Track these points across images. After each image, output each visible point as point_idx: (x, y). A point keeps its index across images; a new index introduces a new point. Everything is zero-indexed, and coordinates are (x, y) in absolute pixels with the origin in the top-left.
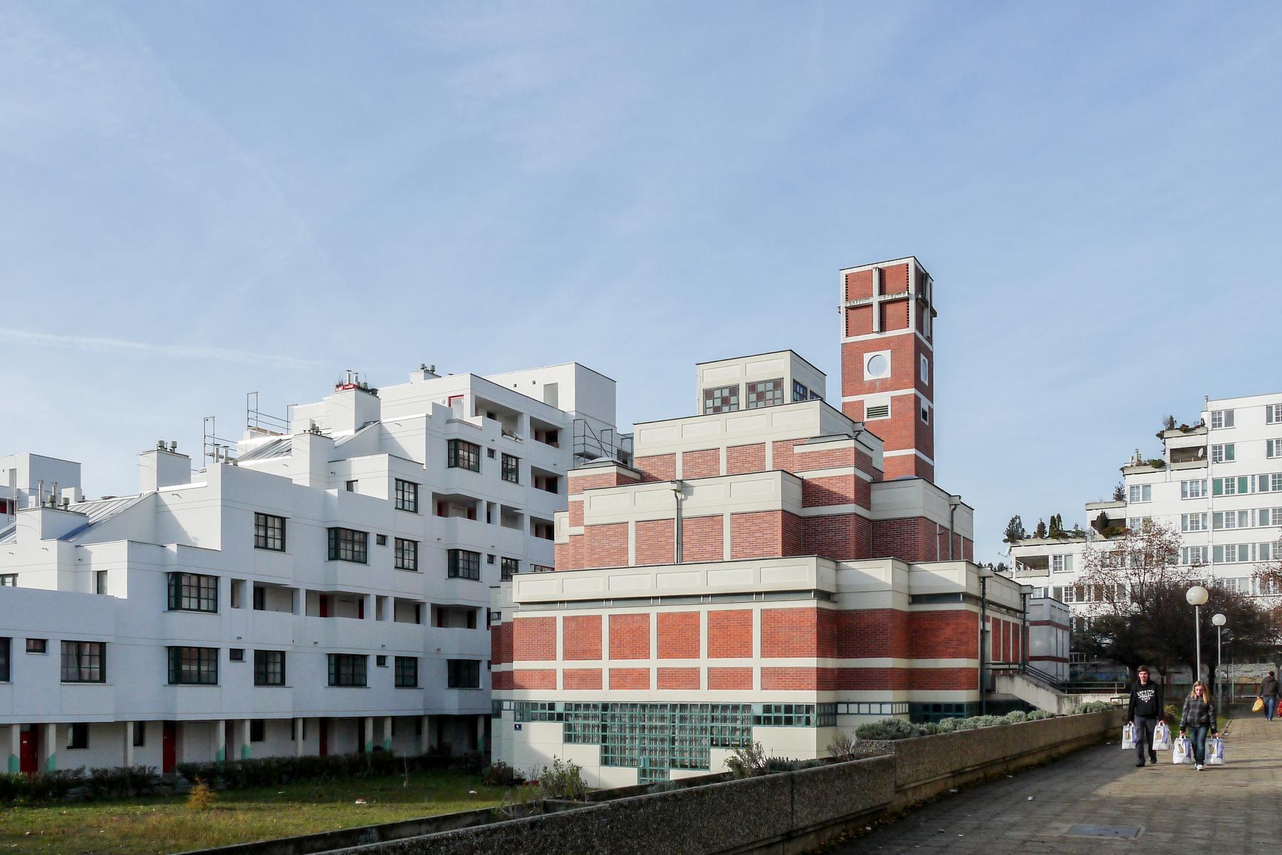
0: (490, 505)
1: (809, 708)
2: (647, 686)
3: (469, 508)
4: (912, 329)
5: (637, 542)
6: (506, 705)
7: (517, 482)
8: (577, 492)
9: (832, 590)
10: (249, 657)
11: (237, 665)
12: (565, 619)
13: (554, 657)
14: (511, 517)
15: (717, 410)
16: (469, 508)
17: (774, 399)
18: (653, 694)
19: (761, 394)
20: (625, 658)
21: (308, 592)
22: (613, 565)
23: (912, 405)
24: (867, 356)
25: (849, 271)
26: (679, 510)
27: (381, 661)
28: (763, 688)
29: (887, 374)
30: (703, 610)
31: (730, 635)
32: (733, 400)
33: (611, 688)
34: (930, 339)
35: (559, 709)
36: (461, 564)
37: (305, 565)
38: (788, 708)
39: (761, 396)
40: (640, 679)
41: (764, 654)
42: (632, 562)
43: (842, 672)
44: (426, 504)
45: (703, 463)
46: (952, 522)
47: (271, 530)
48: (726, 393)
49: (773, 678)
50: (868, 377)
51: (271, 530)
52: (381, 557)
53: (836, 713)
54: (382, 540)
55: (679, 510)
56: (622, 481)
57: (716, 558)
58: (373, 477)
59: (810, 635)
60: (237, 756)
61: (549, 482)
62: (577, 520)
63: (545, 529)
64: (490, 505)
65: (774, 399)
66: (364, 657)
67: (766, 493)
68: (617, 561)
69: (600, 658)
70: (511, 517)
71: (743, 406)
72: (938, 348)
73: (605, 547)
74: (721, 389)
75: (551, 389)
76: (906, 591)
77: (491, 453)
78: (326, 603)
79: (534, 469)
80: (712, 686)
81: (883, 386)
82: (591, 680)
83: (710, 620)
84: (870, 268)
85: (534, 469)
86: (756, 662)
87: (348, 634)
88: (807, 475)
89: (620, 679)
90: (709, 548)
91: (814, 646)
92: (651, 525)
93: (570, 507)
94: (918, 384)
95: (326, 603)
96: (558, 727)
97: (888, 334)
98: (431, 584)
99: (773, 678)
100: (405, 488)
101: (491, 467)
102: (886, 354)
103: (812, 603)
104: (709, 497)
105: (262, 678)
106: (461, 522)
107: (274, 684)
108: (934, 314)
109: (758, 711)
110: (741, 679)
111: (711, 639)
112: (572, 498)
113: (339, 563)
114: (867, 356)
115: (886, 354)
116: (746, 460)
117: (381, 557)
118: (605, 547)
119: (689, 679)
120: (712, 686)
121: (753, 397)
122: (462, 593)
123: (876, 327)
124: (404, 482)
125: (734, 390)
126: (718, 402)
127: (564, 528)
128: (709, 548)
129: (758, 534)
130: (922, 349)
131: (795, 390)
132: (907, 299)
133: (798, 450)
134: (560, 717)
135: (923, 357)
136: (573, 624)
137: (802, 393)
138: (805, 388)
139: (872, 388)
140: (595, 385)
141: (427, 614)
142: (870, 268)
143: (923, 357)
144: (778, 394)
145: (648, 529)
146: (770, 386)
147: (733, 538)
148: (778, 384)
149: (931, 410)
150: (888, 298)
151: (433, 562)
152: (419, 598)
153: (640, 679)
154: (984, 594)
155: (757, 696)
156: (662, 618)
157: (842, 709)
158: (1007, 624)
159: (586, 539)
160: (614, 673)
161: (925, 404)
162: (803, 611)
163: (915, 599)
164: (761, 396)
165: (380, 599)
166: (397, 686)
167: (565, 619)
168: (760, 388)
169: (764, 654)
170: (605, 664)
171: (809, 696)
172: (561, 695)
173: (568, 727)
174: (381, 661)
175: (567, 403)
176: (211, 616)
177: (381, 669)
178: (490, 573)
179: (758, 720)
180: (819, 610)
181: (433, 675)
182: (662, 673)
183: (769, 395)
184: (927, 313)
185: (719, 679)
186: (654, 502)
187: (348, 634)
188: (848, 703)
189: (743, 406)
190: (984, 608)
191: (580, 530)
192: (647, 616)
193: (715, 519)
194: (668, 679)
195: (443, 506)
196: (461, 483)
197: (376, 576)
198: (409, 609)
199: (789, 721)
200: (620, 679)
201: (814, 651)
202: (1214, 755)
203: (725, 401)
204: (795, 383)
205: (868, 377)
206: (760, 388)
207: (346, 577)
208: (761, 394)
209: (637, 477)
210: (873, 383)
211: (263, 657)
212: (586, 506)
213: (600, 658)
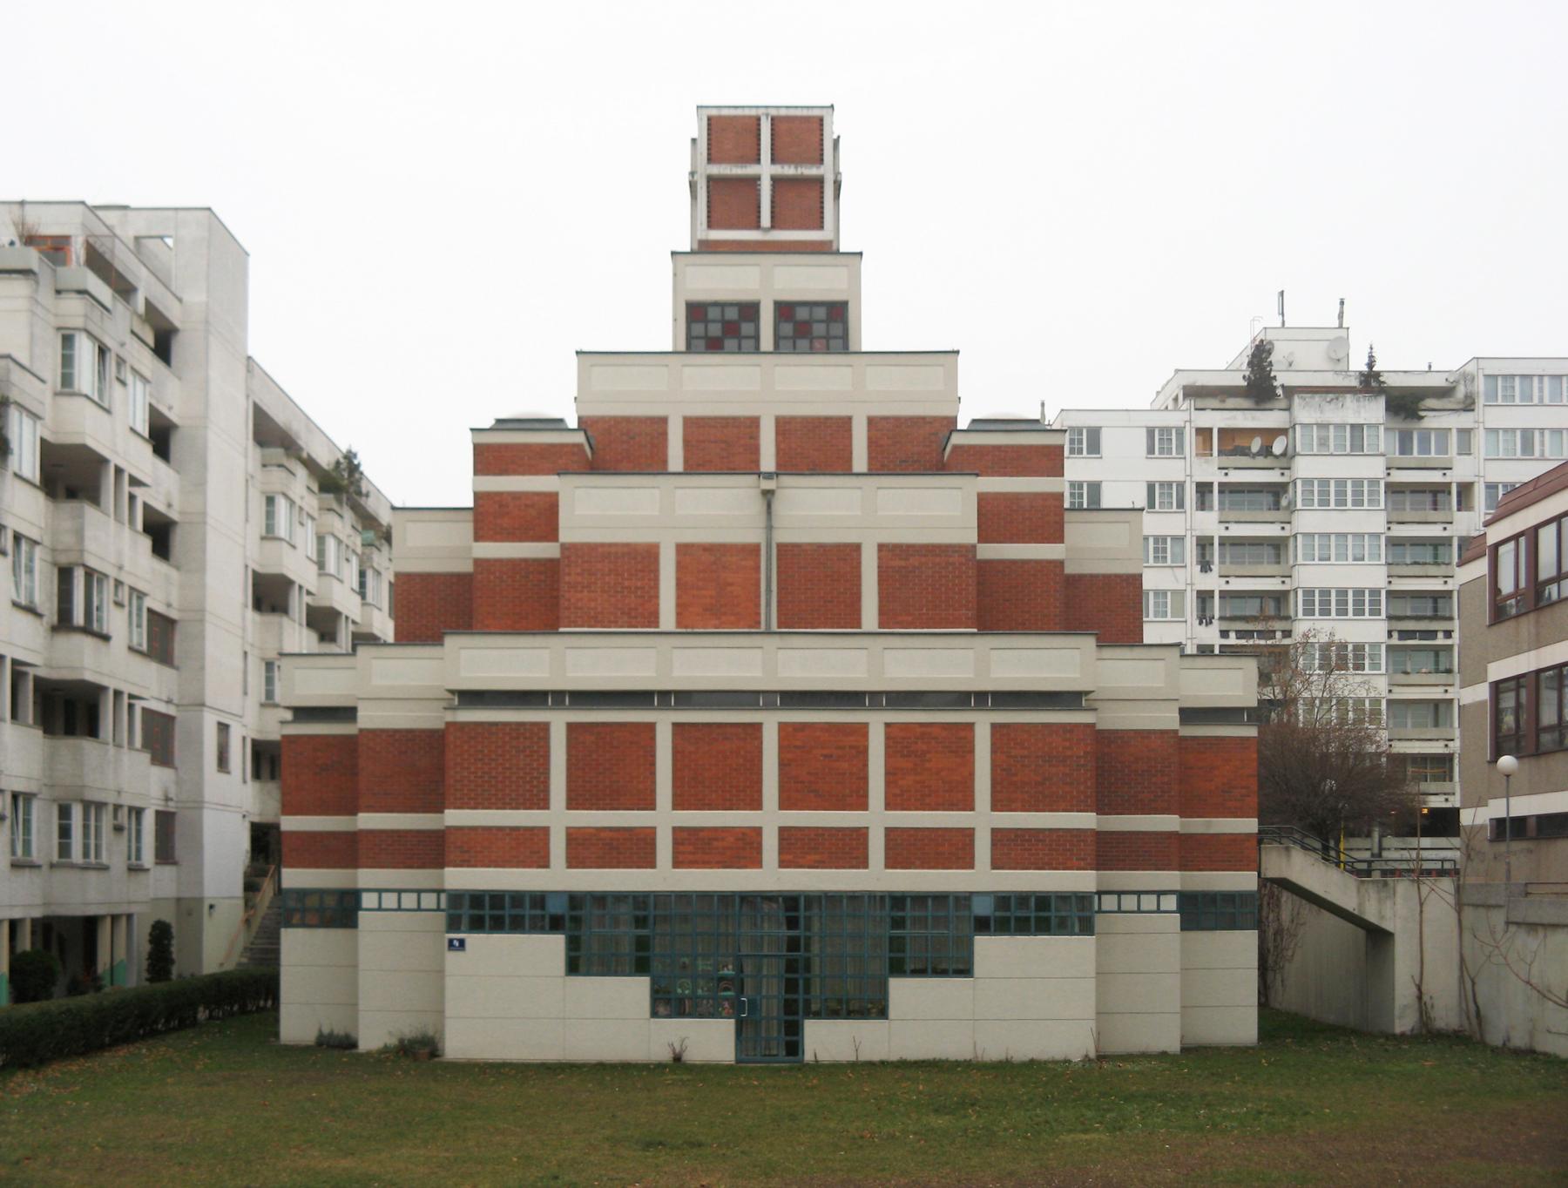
2: (756, 862)
12: (572, 728)
13: (756, 803)
15: (714, 345)
17: (828, 338)
18: (664, 876)
26: (769, 528)
28: (570, 865)
32: (747, 328)
35: (556, 907)
40: (955, 848)
43: (1101, 837)
48: (732, 314)
49: (1013, 849)
65: (828, 338)
68: (634, 613)
71: (767, 341)
74: (722, 305)
80: (574, 861)
83: (889, 738)
86: (983, 819)
99: (1011, 850)
109: (982, 908)
120: (574, 861)
121: (787, 328)
125: (749, 311)
126: (715, 330)
134: (555, 925)
146: (821, 313)
155: (982, 878)
163: (1189, 715)
167: (572, 728)
172: (558, 877)
173: (573, 945)
179: (983, 925)
183: (819, 329)
189: (767, 341)
200: (905, 847)
202: (726, 971)
203: (731, 329)
206: (802, 314)
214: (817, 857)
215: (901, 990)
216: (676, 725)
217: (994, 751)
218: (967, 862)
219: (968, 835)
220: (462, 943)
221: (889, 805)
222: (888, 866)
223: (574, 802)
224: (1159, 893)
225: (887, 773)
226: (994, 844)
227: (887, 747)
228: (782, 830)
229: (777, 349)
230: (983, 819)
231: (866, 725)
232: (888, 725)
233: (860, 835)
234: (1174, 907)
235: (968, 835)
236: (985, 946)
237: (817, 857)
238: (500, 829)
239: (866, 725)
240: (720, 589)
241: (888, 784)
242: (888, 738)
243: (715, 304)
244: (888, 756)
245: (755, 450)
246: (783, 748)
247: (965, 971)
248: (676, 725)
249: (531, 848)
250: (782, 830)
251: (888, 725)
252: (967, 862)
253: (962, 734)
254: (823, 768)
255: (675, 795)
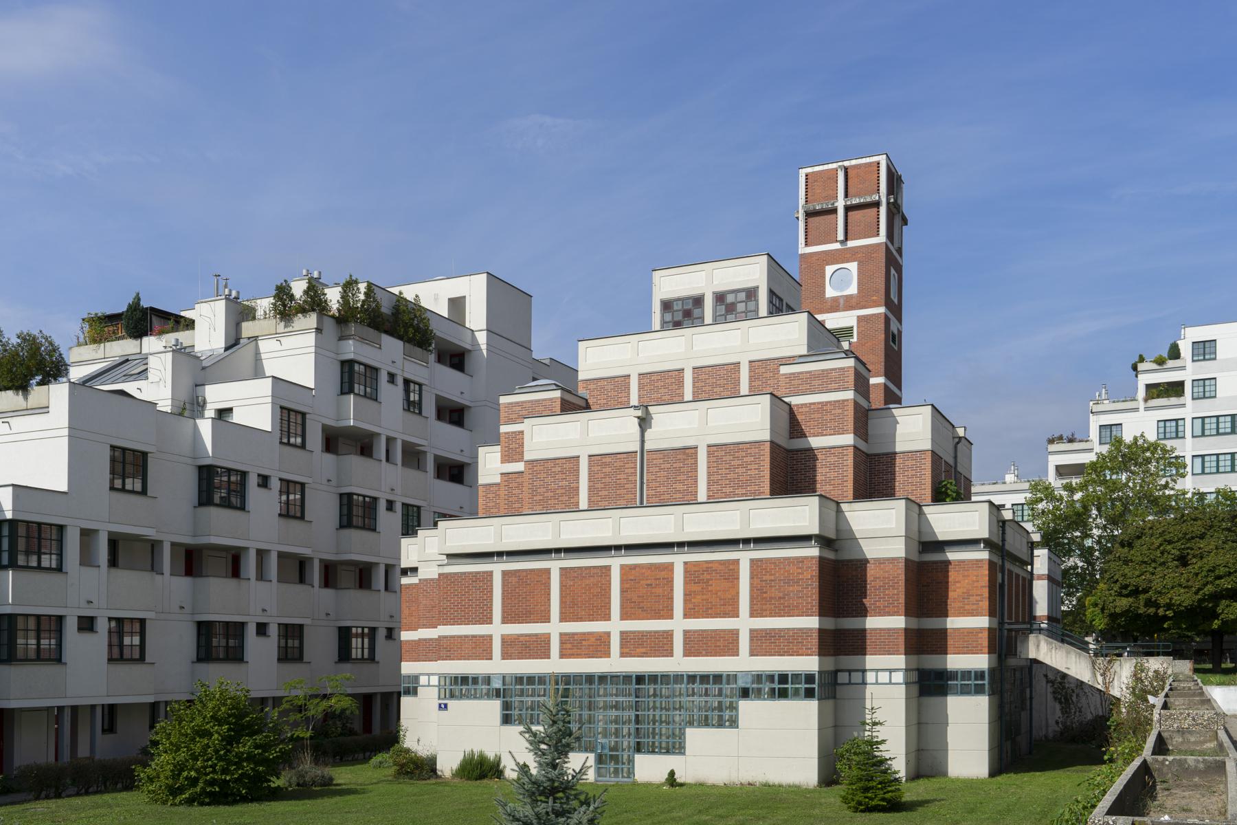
0: (390, 440)
1: (810, 678)
2: (736, 653)
3: (363, 444)
4: (882, 238)
5: (590, 480)
6: (423, 680)
7: (420, 413)
8: (511, 421)
9: (832, 536)
10: (102, 626)
11: (87, 637)
12: (505, 574)
13: (607, 617)
14: (413, 456)
15: (677, 325)
16: (363, 444)
17: (746, 312)
19: (731, 306)
20: (581, 619)
21: (173, 544)
22: (559, 507)
23: (882, 326)
24: (829, 269)
25: (809, 170)
26: (643, 442)
27: (262, 629)
29: (853, 289)
30: (678, 560)
31: (712, 591)
32: (696, 312)
33: (562, 656)
34: (900, 251)
35: (497, 684)
36: (356, 512)
37: (169, 513)
38: (783, 678)
39: (731, 308)
40: (599, 645)
41: (754, 613)
42: (584, 504)
44: (315, 439)
45: (663, 387)
46: (956, 457)
47: (129, 466)
49: (764, 642)
50: (830, 293)
51: (129, 466)
52: (264, 503)
53: (864, 683)
54: (264, 481)
55: (643, 442)
56: (568, 407)
57: (689, 499)
58: (253, 406)
59: (812, 593)
60: (83, 751)
61: (453, 414)
62: (513, 450)
63: (456, 472)
64: (390, 440)
66: (242, 625)
67: (750, 420)
68: (564, 502)
69: (548, 620)
70: (413, 456)
71: (708, 318)
72: (906, 262)
73: (549, 487)
74: (683, 300)
75: (457, 304)
76: (916, 538)
77: (392, 378)
78: (192, 561)
79: (439, 399)
80: (688, 652)
81: (848, 304)
82: (538, 647)
84: (834, 166)
85: (439, 399)
86: (744, 623)
87: (222, 599)
88: (795, 401)
89: (572, 645)
90: (680, 487)
91: (816, 603)
92: (608, 460)
93: (502, 439)
94: (888, 303)
95: (192, 561)
96: (496, 705)
97: (851, 244)
98: (320, 537)
99: (764, 642)
100: (291, 417)
101: (392, 395)
102: (853, 267)
103: (813, 551)
104: (676, 426)
105: (117, 655)
106: (355, 462)
107: (132, 660)
108: (905, 221)
110: (725, 644)
111: (688, 596)
112: (504, 429)
113: (213, 511)
114: (829, 269)
115: (853, 267)
116: (716, 383)
117: (264, 503)
118: (549, 487)
119: (660, 644)
120: (688, 652)
122: (357, 546)
123: (841, 237)
124: (289, 410)
125: (698, 301)
127: (490, 465)
128: (680, 487)
129: (740, 470)
130: (893, 261)
131: (770, 302)
132: (877, 204)
133: (784, 370)
134: (498, 694)
135: (893, 271)
136: (514, 580)
137: (779, 306)
138: (781, 300)
139: (835, 306)
140: (508, 300)
141: (316, 574)
142: (834, 166)
143: (893, 271)
144: (751, 305)
145: (606, 464)
146: (742, 296)
147: (709, 474)
148: (751, 293)
149: (900, 332)
150: (856, 201)
151: (323, 508)
152: (305, 551)
153: (599, 645)
154: (1003, 540)
155: (744, 663)
156: (691, 571)
157: (842, 678)
158: (1017, 576)
159: (527, 476)
160: (565, 638)
161: (894, 327)
162: (801, 560)
164: (731, 308)
165: (262, 554)
166: (279, 660)
167: (505, 574)
168: (730, 299)
169: (754, 613)
170: (615, 626)
171: (810, 663)
172: (498, 666)
173: (506, 706)
174: (262, 629)
175: (476, 318)
176: (56, 578)
177: (262, 639)
178: (389, 521)
179: (745, 693)
180: (821, 559)
181: (321, 645)
182: (565, 638)
183: (741, 307)
184: (898, 221)
185: (697, 644)
186: (610, 431)
187: (222, 599)
188: (850, 671)
189: (708, 318)
190: (1003, 559)
191: (519, 467)
192: (608, 568)
193: (689, 452)
194: (573, 646)
195: (333, 441)
196: (351, 413)
197: (258, 525)
198: (295, 568)
199: (783, 694)
200: (572, 645)
201: (816, 609)
203: (687, 314)
204: (772, 293)
205: (830, 293)
206: (730, 299)
207: (221, 527)
208: (731, 306)
209: (583, 404)
210: (835, 299)
211: (120, 625)
212: (526, 437)
213: (548, 620)
214: (643, 650)
215: (694, 736)
216: (752, 561)
217: (752, 578)
218: (546, 655)
219: (735, 634)
220: (446, 705)
221: (686, 616)
222: (685, 655)
223: (505, 620)
224: (891, 671)
225: (685, 595)
226: (751, 639)
227: (685, 577)
228: (622, 633)
229: (716, 322)
230: (744, 623)
231: (672, 564)
232: (685, 563)
233: (668, 635)
234: (901, 681)
235: (735, 634)
236: (746, 707)
237: (643, 650)
238: (466, 636)
239: (672, 564)
240: (620, 481)
241: (686, 601)
242: (686, 571)
243: (678, 299)
244: (686, 583)
245: (737, 382)
246: (623, 581)
247: (734, 723)
248: (752, 561)
249: (480, 648)
250: (622, 633)
251: (685, 563)
252: (546, 655)
253: (663, 574)
254: (647, 595)
255: (561, 613)
